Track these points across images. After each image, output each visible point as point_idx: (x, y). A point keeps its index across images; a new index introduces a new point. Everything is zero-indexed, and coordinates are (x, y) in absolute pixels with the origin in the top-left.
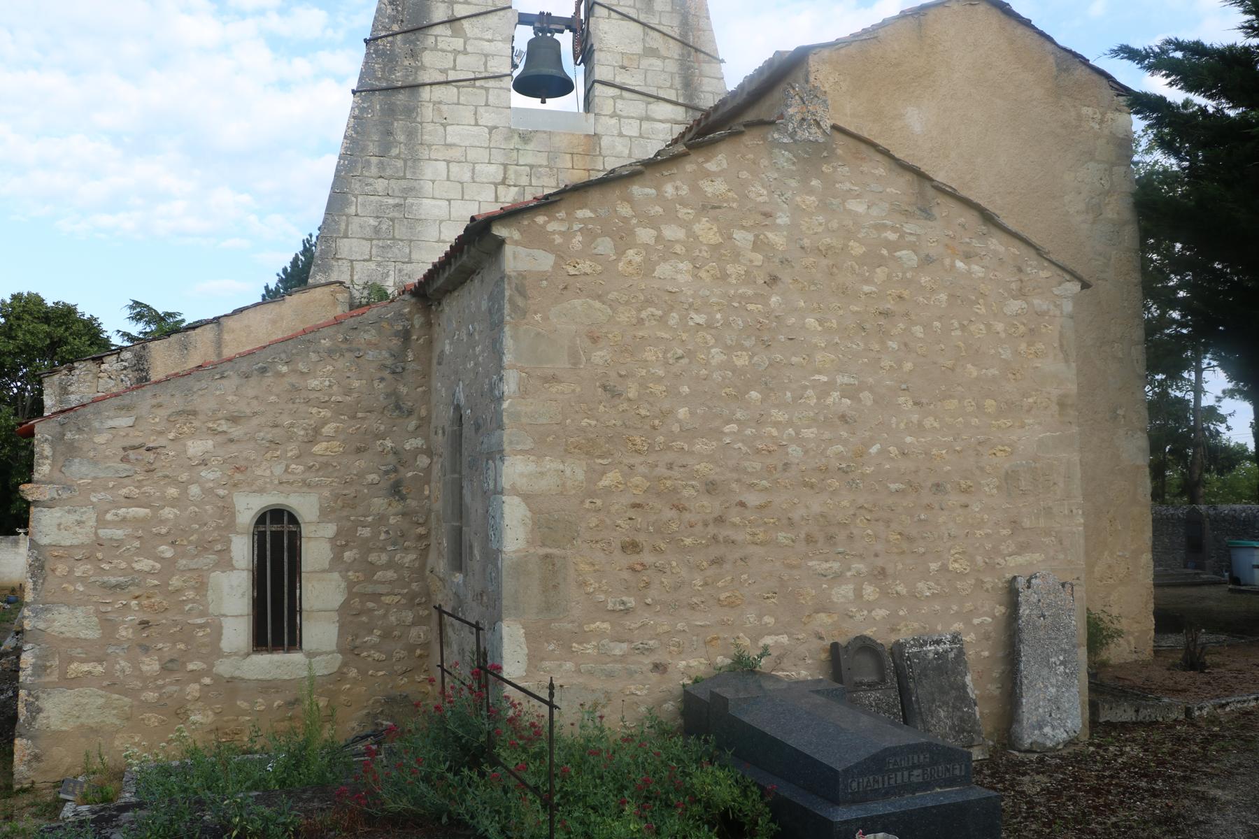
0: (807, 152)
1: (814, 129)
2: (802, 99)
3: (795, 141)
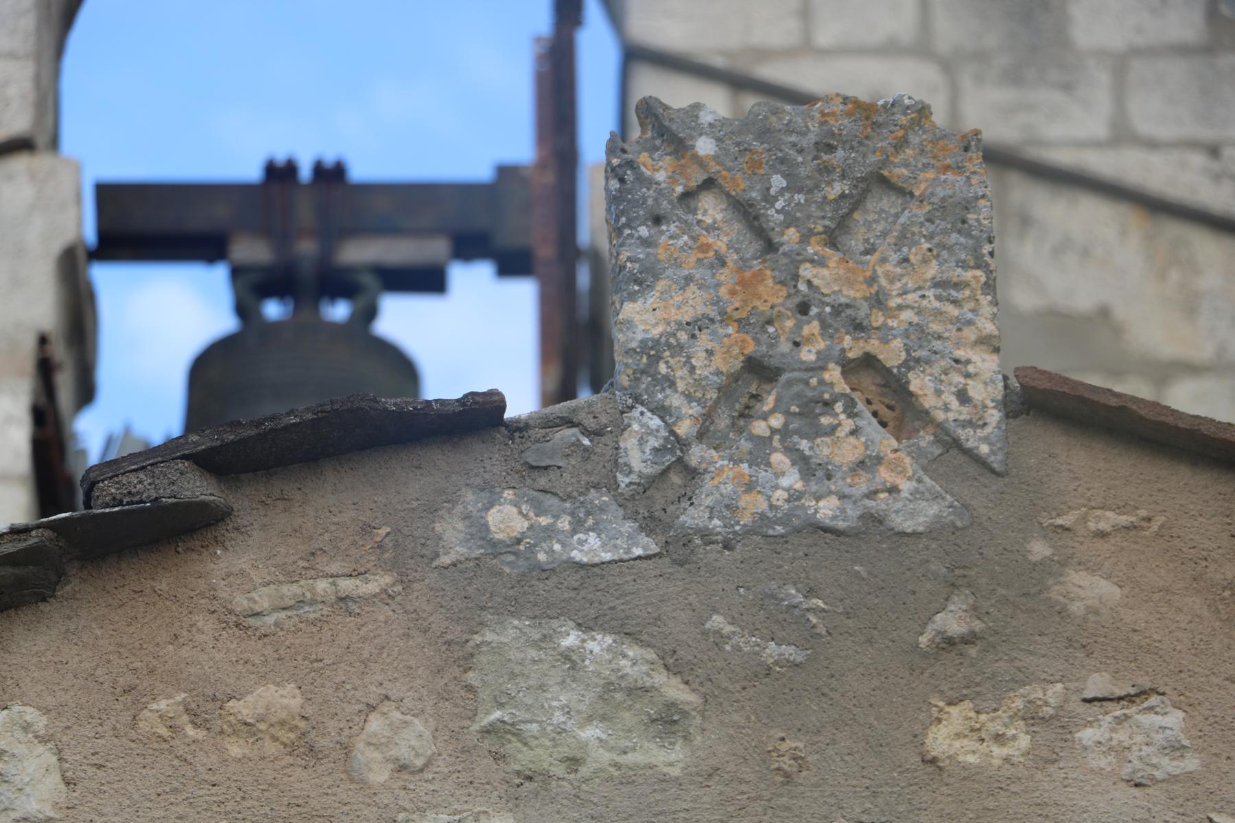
0: (783, 621)
1: (850, 439)
2: (746, 212)
3: (679, 549)
